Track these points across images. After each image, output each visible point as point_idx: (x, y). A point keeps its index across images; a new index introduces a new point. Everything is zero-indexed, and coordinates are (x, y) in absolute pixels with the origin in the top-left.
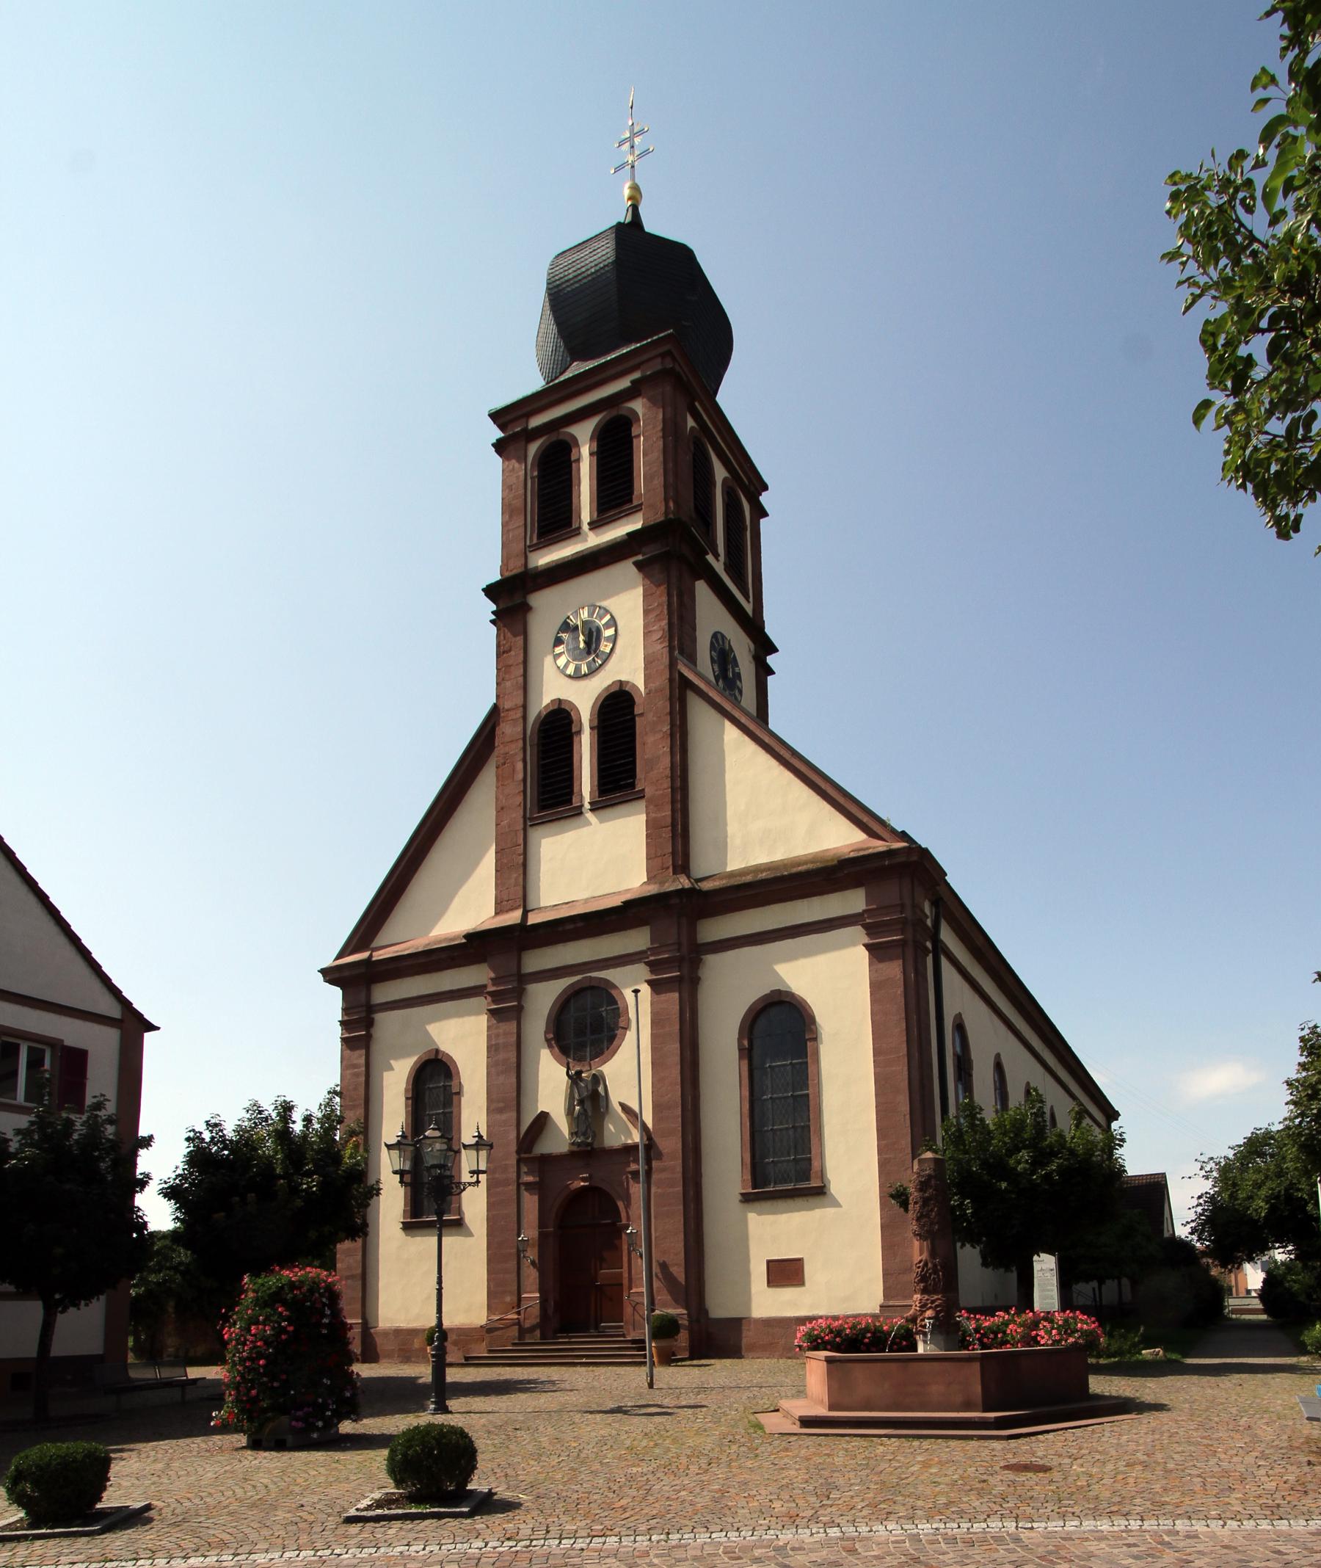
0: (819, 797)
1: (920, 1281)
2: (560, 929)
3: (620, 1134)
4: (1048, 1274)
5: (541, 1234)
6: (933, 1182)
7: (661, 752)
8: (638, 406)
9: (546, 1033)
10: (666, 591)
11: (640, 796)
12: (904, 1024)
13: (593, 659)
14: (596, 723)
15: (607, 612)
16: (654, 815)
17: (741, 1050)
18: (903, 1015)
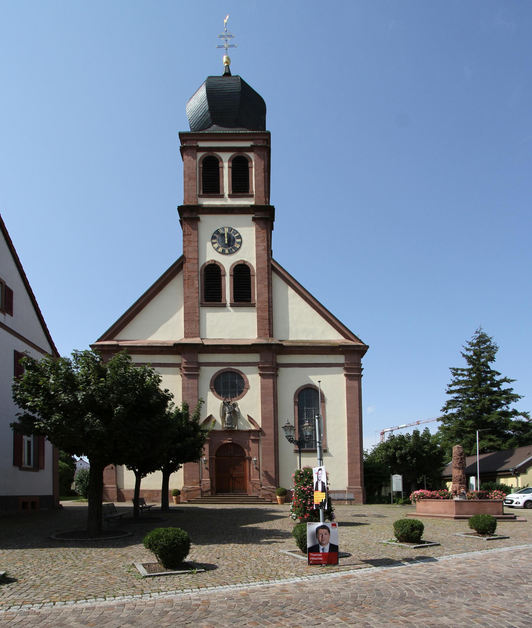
0: (326, 322)
1: (459, 481)
2: (219, 348)
3: (243, 425)
4: (399, 481)
5: (209, 458)
6: (463, 454)
7: (264, 292)
8: (252, 155)
9: (210, 386)
10: (266, 232)
11: (253, 306)
12: (358, 401)
13: (231, 249)
14: (232, 274)
15: (237, 232)
16: (261, 314)
17: (295, 402)
18: (358, 399)
